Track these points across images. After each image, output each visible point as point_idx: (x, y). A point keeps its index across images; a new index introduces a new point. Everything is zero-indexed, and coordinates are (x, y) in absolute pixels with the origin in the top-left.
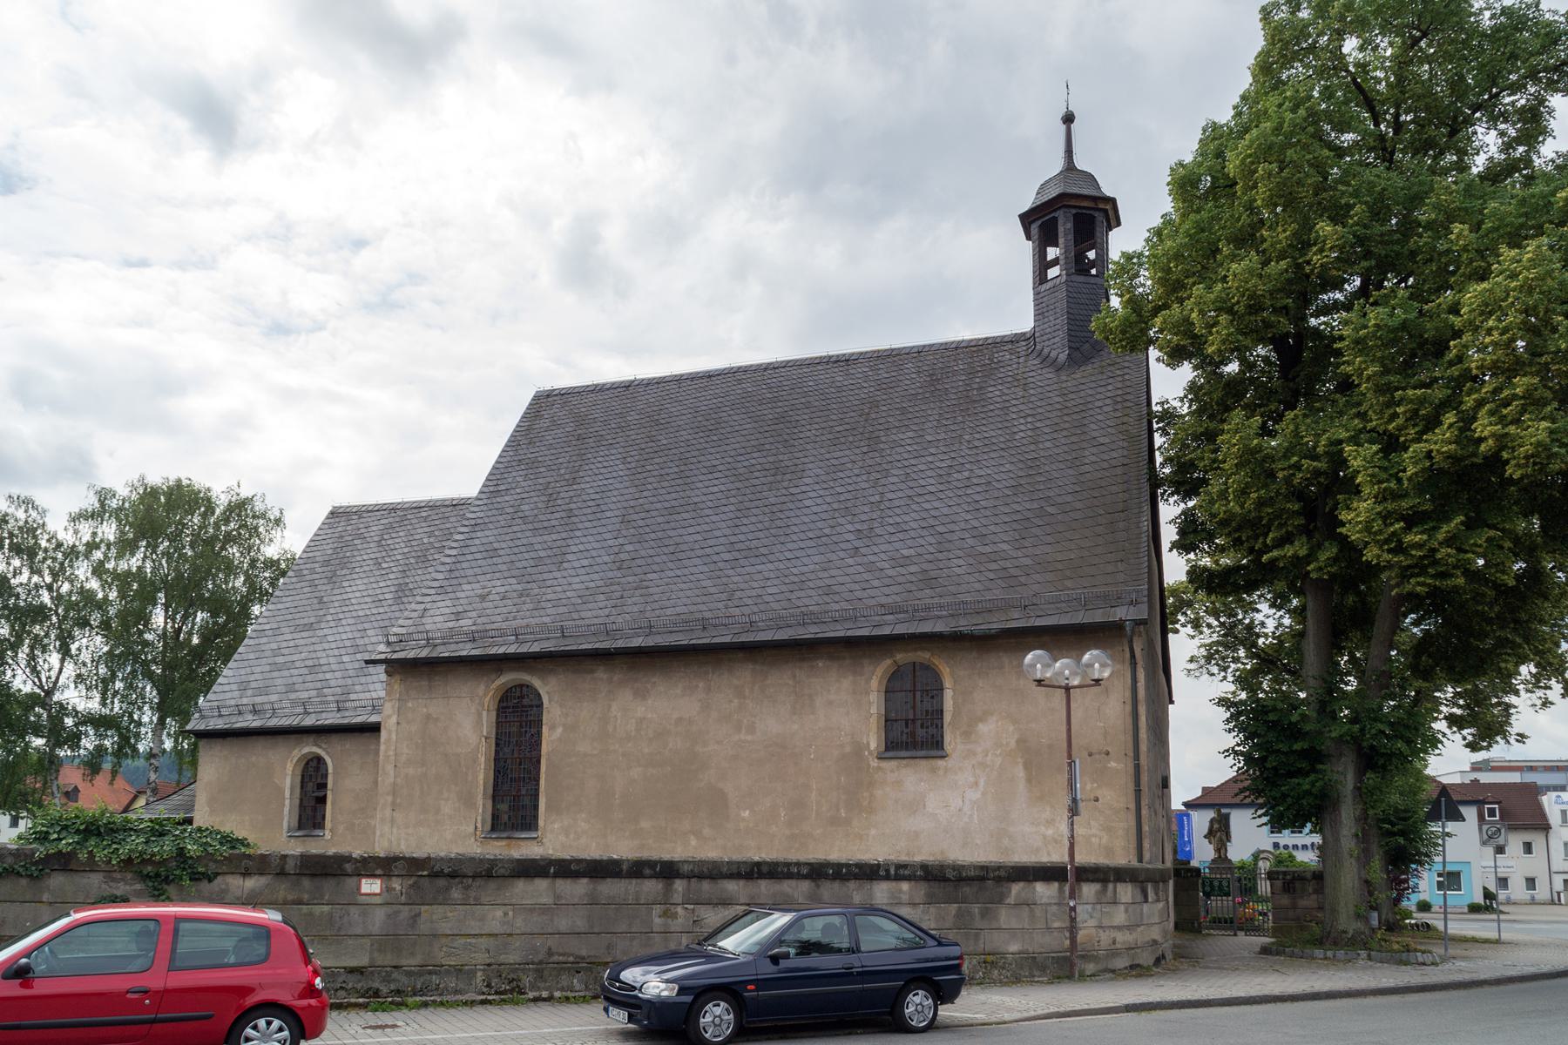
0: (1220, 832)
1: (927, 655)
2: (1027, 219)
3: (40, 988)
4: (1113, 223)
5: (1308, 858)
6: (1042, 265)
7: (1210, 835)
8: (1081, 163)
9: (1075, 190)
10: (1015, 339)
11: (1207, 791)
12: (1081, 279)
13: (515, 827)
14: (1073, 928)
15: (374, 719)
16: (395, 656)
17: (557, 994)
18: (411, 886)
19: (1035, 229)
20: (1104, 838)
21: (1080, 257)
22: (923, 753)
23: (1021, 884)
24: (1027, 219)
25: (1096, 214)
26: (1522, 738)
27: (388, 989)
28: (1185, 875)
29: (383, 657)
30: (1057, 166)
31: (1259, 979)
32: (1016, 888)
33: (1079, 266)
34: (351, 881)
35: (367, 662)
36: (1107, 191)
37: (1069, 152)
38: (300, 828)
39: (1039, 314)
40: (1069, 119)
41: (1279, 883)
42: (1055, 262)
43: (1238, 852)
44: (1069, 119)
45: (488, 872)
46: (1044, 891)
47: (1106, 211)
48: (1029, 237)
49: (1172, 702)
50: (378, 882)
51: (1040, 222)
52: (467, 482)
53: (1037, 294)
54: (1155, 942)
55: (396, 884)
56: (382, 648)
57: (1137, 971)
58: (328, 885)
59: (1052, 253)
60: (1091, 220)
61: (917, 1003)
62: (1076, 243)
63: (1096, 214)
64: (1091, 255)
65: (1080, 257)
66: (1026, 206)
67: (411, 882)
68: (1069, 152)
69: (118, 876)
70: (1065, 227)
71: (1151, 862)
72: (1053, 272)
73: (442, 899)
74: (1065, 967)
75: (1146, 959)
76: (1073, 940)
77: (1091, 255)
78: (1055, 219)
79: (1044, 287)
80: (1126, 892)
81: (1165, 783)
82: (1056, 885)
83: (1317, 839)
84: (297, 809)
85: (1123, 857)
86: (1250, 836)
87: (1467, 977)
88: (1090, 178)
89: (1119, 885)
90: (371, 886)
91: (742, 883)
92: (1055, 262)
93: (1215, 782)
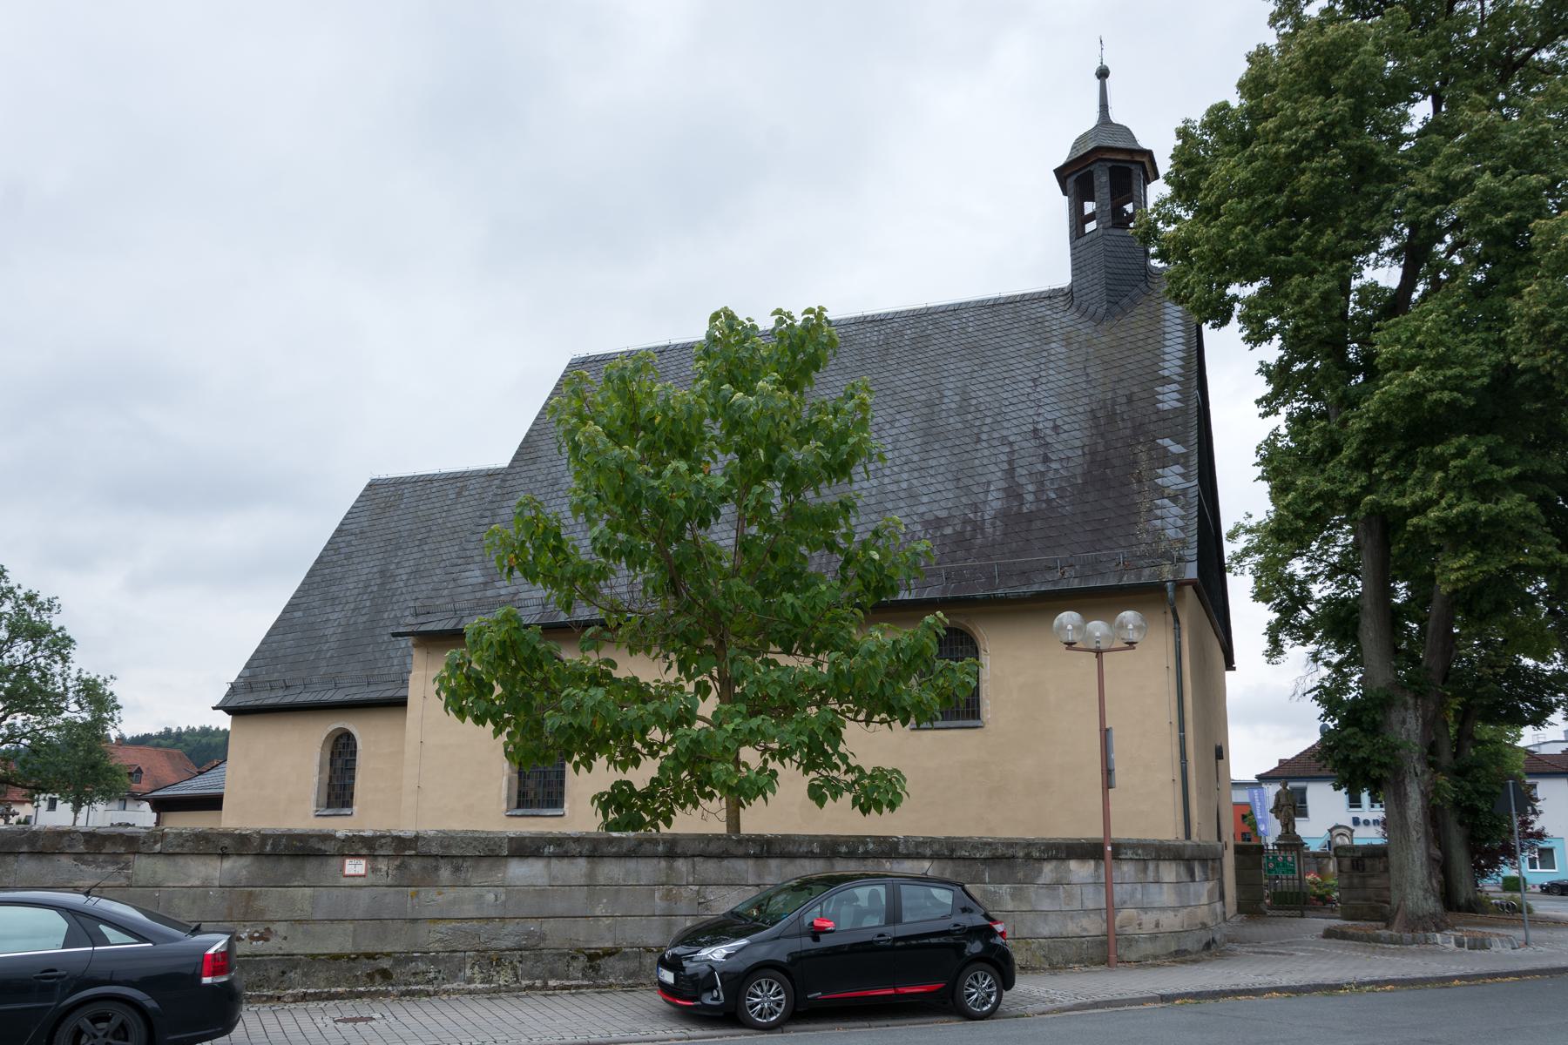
0: (1291, 807)
1: (963, 621)
2: (1062, 174)
3: (826, 941)
4: (1150, 175)
5: (1369, 836)
6: (1078, 220)
7: (1277, 810)
8: (1116, 117)
9: (1110, 143)
10: (1051, 295)
11: (1283, 763)
12: (1119, 232)
13: (540, 805)
14: (1111, 910)
15: (401, 694)
16: (422, 628)
17: (552, 983)
18: (398, 867)
19: (1070, 182)
20: (1148, 811)
21: (1117, 211)
22: (959, 723)
23: (1054, 863)
24: (1062, 174)
25: (1133, 167)
26: (1275, 649)
27: (372, 974)
28: (1249, 852)
29: (409, 629)
30: (1091, 120)
31: (1407, 960)
32: (1049, 870)
33: (1119, 220)
34: (335, 862)
35: (395, 635)
36: (1144, 143)
37: (1104, 107)
38: (329, 806)
39: (1077, 268)
40: (1103, 74)
41: (1347, 863)
42: (1091, 217)
43: (1313, 830)
44: (1103, 74)
45: (525, 849)
46: (1080, 870)
47: (1143, 164)
48: (1065, 193)
49: (1230, 665)
50: (363, 862)
51: (1076, 176)
52: (498, 453)
53: (1073, 248)
54: (1204, 926)
55: (383, 865)
56: (410, 620)
57: (1180, 956)
58: (311, 866)
59: (1089, 207)
60: (1127, 174)
61: (978, 988)
62: (1113, 198)
63: (1133, 167)
64: (1129, 208)
65: (1117, 211)
66: (1061, 159)
67: (397, 862)
68: (1104, 107)
69: (90, 858)
70: (1102, 180)
71: (1202, 834)
72: (1091, 226)
73: (428, 879)
74: (1104, 953)
75: (1189, 944)
76: (1109, 921)
77: (1129, 208)
78: (1091, 173)
79: (1082, 241)
80: (1169, 872)
81: (1220, 753)
82: (1092, 863)
83: (1378, 813)
84: (325, 789)
85: (1167, 830)
86: (1328, 812)
87: (1545, 964)
88: (1125, 132)
89: (1162, 864)
90: (355, 867)
91: (751, 862)
92: (1091, 217)
93: (1290, 754)
